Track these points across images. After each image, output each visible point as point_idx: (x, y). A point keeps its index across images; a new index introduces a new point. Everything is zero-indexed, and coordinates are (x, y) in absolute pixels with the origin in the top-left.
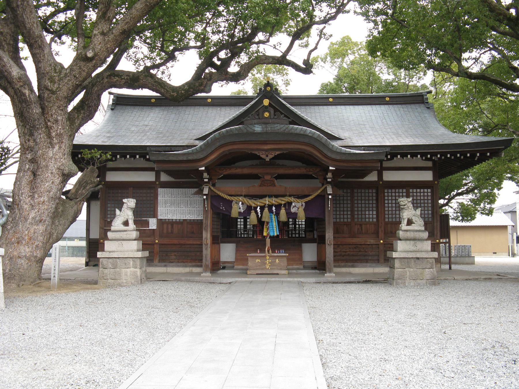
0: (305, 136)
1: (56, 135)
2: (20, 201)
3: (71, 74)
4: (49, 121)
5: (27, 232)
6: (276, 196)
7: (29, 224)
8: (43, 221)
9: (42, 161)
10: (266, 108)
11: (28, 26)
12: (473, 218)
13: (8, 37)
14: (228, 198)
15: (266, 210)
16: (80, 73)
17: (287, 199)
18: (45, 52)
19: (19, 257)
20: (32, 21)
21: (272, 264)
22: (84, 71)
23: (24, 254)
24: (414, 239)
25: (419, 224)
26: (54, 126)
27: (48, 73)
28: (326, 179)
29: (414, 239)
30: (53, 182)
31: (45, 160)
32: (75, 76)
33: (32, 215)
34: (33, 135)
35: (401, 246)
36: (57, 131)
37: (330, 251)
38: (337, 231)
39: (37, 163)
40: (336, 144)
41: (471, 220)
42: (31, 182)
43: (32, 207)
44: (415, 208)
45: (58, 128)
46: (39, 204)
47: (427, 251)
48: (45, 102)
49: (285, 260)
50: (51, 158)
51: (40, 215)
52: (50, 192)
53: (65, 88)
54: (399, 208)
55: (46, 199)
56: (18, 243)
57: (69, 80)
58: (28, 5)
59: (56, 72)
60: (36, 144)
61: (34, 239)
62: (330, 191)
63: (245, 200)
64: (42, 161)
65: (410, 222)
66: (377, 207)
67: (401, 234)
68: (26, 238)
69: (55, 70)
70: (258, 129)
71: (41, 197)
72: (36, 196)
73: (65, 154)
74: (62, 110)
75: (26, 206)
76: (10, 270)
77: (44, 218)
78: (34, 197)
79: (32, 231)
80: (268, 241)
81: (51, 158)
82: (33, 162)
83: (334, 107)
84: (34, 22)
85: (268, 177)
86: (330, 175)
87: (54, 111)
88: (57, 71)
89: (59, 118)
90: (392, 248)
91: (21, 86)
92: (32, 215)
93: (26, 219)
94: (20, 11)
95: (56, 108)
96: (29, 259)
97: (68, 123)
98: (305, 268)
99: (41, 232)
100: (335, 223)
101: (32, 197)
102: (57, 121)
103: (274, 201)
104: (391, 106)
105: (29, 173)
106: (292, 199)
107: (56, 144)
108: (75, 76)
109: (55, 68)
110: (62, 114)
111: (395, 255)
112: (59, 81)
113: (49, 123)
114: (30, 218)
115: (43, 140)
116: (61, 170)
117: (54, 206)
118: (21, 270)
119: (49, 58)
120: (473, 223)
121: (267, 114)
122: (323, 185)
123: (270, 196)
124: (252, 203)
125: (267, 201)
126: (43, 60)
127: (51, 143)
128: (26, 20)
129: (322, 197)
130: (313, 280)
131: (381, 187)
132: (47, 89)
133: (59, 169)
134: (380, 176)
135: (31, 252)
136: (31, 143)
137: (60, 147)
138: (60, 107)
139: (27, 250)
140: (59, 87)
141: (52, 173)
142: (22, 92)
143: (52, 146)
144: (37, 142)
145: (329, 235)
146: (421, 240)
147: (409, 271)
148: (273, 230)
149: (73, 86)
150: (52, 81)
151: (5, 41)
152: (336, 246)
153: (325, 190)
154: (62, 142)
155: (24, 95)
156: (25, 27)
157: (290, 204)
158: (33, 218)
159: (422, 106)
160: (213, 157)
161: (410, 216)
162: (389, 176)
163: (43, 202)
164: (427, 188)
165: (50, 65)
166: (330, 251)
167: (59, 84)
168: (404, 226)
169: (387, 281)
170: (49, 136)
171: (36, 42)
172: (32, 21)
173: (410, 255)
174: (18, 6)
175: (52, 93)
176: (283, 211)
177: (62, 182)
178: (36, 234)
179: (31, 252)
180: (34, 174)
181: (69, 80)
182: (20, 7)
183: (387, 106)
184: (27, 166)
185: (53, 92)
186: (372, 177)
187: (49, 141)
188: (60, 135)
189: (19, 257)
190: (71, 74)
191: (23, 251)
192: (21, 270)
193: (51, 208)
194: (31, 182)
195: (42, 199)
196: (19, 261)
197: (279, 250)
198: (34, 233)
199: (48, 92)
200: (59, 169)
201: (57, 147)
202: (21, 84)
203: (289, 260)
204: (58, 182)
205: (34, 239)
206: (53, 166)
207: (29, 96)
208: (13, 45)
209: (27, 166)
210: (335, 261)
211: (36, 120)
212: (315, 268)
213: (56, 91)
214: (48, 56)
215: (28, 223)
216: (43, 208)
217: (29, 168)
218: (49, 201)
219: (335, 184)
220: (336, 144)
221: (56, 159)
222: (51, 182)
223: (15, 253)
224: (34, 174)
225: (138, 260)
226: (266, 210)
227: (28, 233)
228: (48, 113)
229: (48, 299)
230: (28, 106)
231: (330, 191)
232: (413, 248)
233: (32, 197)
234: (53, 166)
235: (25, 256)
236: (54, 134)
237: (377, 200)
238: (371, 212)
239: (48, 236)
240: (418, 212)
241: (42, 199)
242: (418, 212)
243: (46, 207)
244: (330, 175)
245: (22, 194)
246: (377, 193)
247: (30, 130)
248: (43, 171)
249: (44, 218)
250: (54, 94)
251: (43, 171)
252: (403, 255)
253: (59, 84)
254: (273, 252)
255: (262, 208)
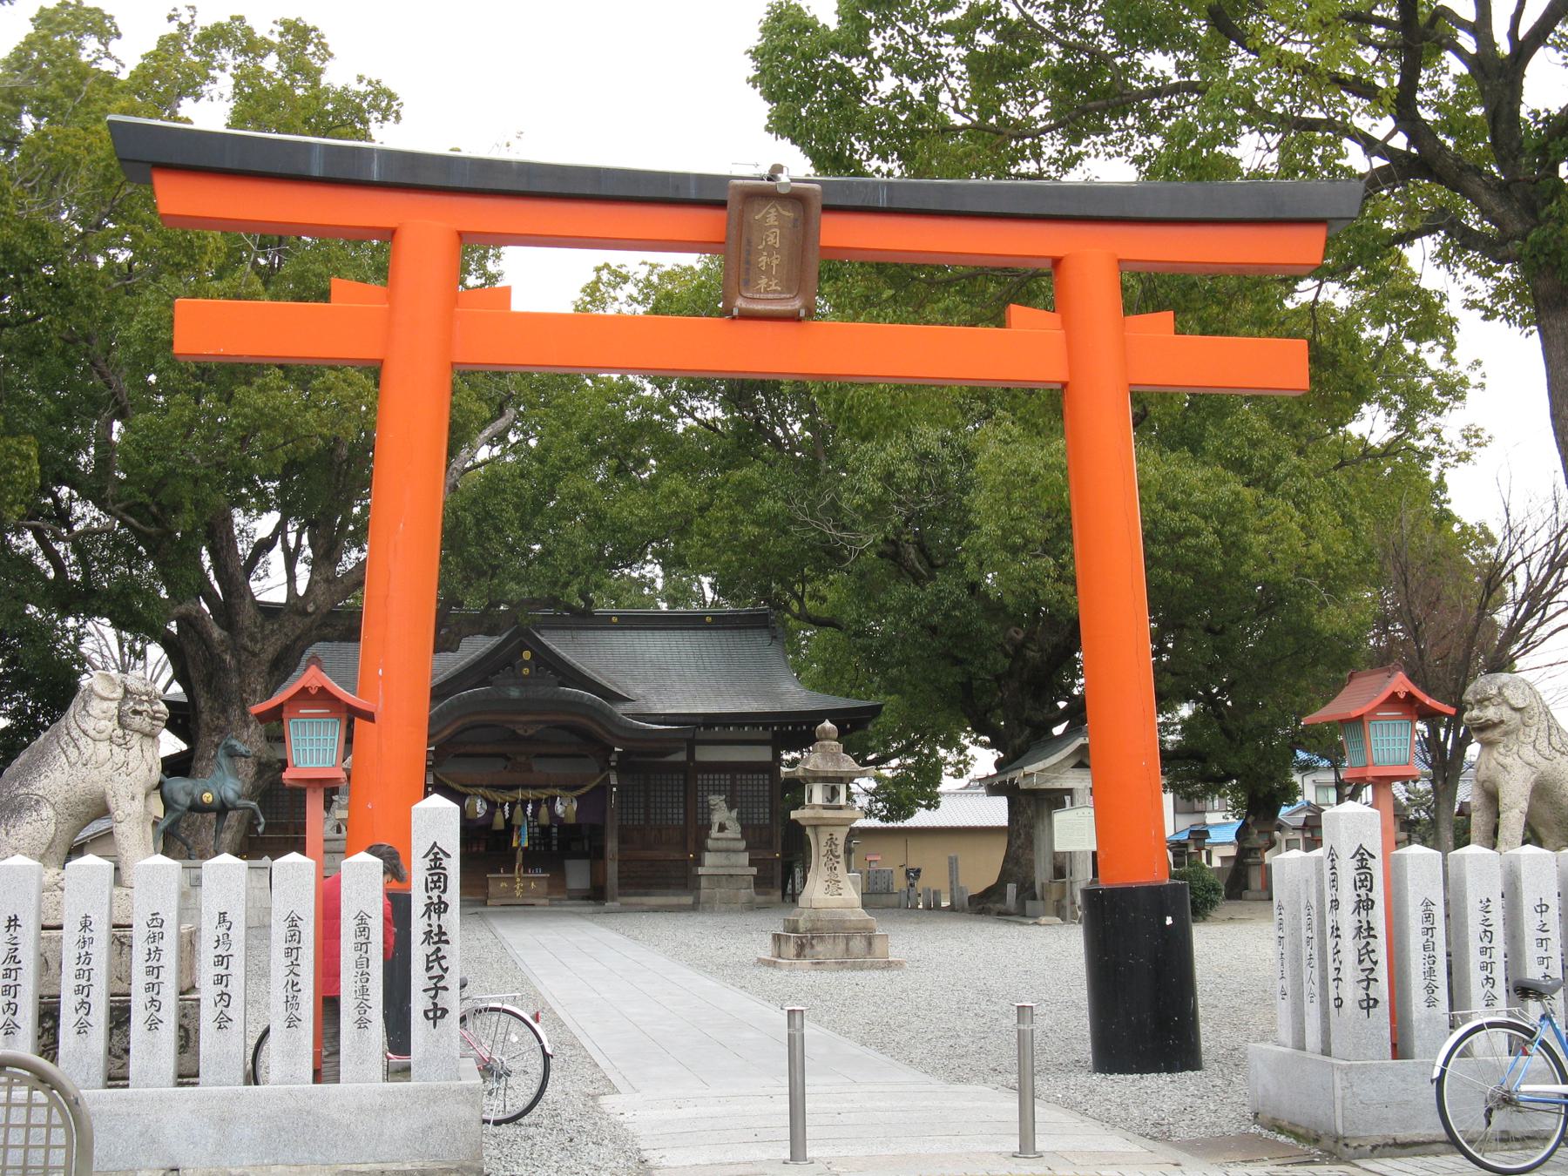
0: (577, 703)
6: (534, 787)
10: (526, 664)
12: (911, 814)
14: (462, 789)
15: (519, 807)
17: (550, 792)
21: (525, 889)
24: (727, 851)
25: (734, 831)
28: (608, 762)
29: (727, 851)
35: (709, 858)
37: (612, 868)
38: (623, 840)
40: (620, 709)
41: (906, 817)
44: (731, 808)
47: (742, 867)
49: (545, 883)
53: (271, 649)
54: (709, 811)
60: (230, 723)
62: (614, 780)
63: (488, 793)
65: (722, 828)
66: (685, 803)
67: (710, 842)
70: (515, 693)
80: (520, 854)
83: (619, 633)
85: (522, 759)
86: (614, 757)
90: (699, 862)
98: (570, 898)
100: (621, 827)
103: (530, 794)
104: (714, 633)
106: (558, 792)
111: (701, 871)
120: (910, 823)
121: (526, 671)
122: (602, 771)
123: (525, 787)
124: (497, 797)
125: (520, 794)
129: (603, 788)
130: (590, 909)
131: (692, 771)
134: (691, 754)
136: (222, 722)
145: (612, 846)
146: (735, 851)
147: (719, 892)
148: (521, 841)
150: (253, 638)
152: (622, 862)
153: (607, 778)
155: (224, 661)
157: (553, 799)
159: (765, 633)
160: (446, 732)
161: (722, 820)
162: (705, 754)
164: (763, 772)
166: (612, 868)
168: (714, 833)
169: (694, 908)
173: (721, 871)
176: (544, 810)
183: (706, 633)
185: (254, 654)
186: (681, 757)
197: (533, 868)
203: (550, 886)
210: (620, 886)
212: (588, 898)
219: (621, 770)
220: (620, 709)
226: (519, 807)
231: (614, 780)
232: (725, 862)
237: (685, 791)
238: (37, 1157)
240: (734, 814)
242: (734, 814)
244: (614, 757)
246: (685, 780)
252: (711, 871)
254: (526, 871)
255: (512, 806)
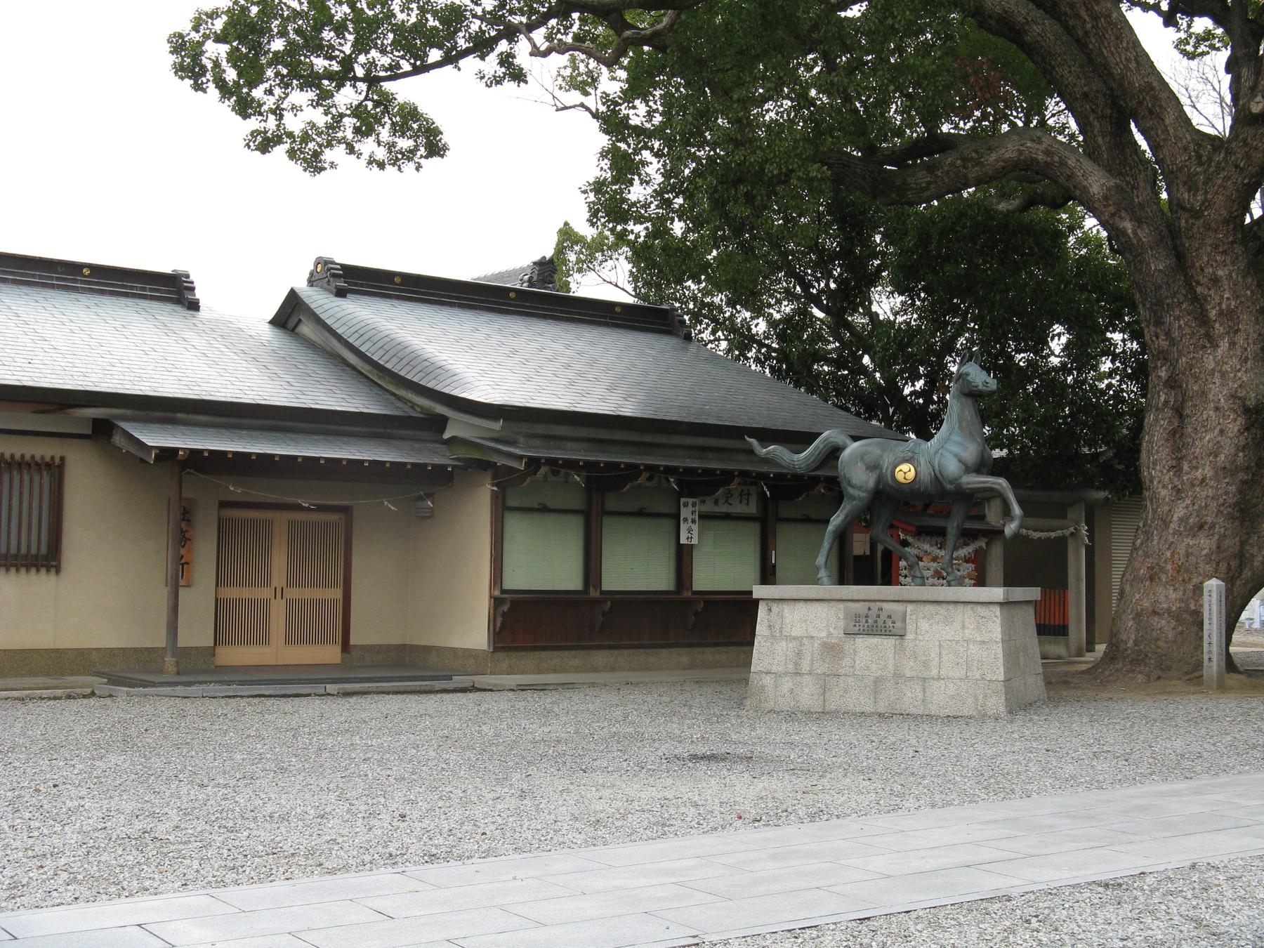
1: (1221, 313)
2: (1152, 481)
3: (1226, 162)
4: (1198, 283)
5: (1168, 554)
7: (1174, 534)
8: (1206, 527)
9: (1191, 381)
11: (1117, 71)
13: (1101, 101)
16: (1248, 156)
18: (1167, 122)
19: (1155, 613)
20: (1123, 57)
22: (1256, 149)
23: (1165, 606)
26: (1212, 292)
27: (1180, 169)
30: (1222, 431)
31: (1196, 378)
32: (1237, 166)
33: (1179, 512)
34: (1163, 323)
36: (1220, 304)
39: (1181, 387)
42: (1174, 435)
43: (1178, 491)
45: (1222, 297)
46: (1193, 485)
48: (1184, 240)
50: (1212, 373)
51: (1198, 511)
52: (1216, 456)
53: (1220, 200)
55: (1208, 472)
56: (1151, 579)
57: (1227, 178)
58: (1110, 23)
59: (1200, 164)
61: (1187, 571)
64: (1191, 381)
68: (1169, 567)
69: (1199, 156)
71: (1196, 468)
72: (1186, 467)
73: (1246, 360)
74: (1224, 252)
75: (1164, 492)
76: (1136, 643)
77: (1209, 520)
78: (1181, 470)
79: (1182, 552)
81: (1212, 373)
82: (1172, 388)
84: (1128, 60)
87: (1206, 259)
88: (1204, 159)
89: (1220, 273)
91: (1113, 215)
92: (1179, 512)
93: (1166, 524)
94: (1093, 43)
95: (1209, 249)
96: (1177, 617)
97: (1249, 280)
99: (1204, 552)
101: (1177, 469)
102: (1215, 281)
105: (1168, 413)
107: (1221, 337)
108: (1237, 166)
109: (1197, 152)
110: (1228, 261)
112: (1205, 183)
113: (1199, 290)
114: (1175, 519)
115: (1187, 331)
116: (1240, 398)
117: (1233, 489)
118: (1161, 643)
119: (1179, 134)
126: (1165, 140)
127: (1208, 336)
128: (1110, 59)
132: (1184, 209)
133: (1233, 396)
135: (1181, 600)
137: (1233, 344)
138: (1217, 247)
139: (1173, 596)
140: (1206, 200)
141: (1217, 409)
142: (1117, 229)
143: (1211, 341)
144: (1173, 339)
149: (1237, 190)
151: (1093, 111)
154: (1236, 332)
156: (1112, 75)
158: (1181, 520)
163: (1203, 480)
165: (1185, 149)
167: (1206, 192)
170: (1203, 320)
171: (1140, 103)
172: (1123, 57)
174: (1086, 33)
175: (1193, 217)
177: (1247, 429)
178: (1192, 559)
179: (1181, 600)
180: (1179, 412)
181: (1227, 178)
182: (1091, 35)
184: (1162, 398)
185: (1196, 214)
187: (1202, 331)
188: (1229, 315)
189: (1155, 613)
190: (1226, 162)
191: (1162, 598)
192: (1161, 643)
193: (1226, 493)
194: (1173, 433)
195: (1199, 474)
196: (1155, 621)
198: (1188, 555)
199: (1187, 215)
200: (1233, 396)
201: (1224, 345)
202: (1112, 209)
204: (1236, 429)
205: (1187, 571)
206: (1218, 392)
207: (1135, 233)
208: (1111, 117)
209: (1162, 398)
211: (1160, 287)
213: (1201, 211)
214: (1176, 130)
215: (1171, 531)
216: (1204, 494)
217: (1166, 402)
218: (1216, 478)
221: (1223, 374)
222: (1216, 431)
223: (1146, 604)
224: (1179, 412)
225: (997, 610)
227: (1172, 555)
228: (1193, 265)
229: (1189, 706)
230: (1136, 256)
233: (1177, 469)
234: (1218, 392)
235: (1168, 610)
236: (1214, 312)
239: (1234, 564)
241: (1199, 474)
243: (1210, 492)
245: (1155, 463)
247: (1155, 312)
248: (1195, 406)
249: (1209, 520)
250: (1198, 218)
251: (1195, 406)
253: (1206, 192)
